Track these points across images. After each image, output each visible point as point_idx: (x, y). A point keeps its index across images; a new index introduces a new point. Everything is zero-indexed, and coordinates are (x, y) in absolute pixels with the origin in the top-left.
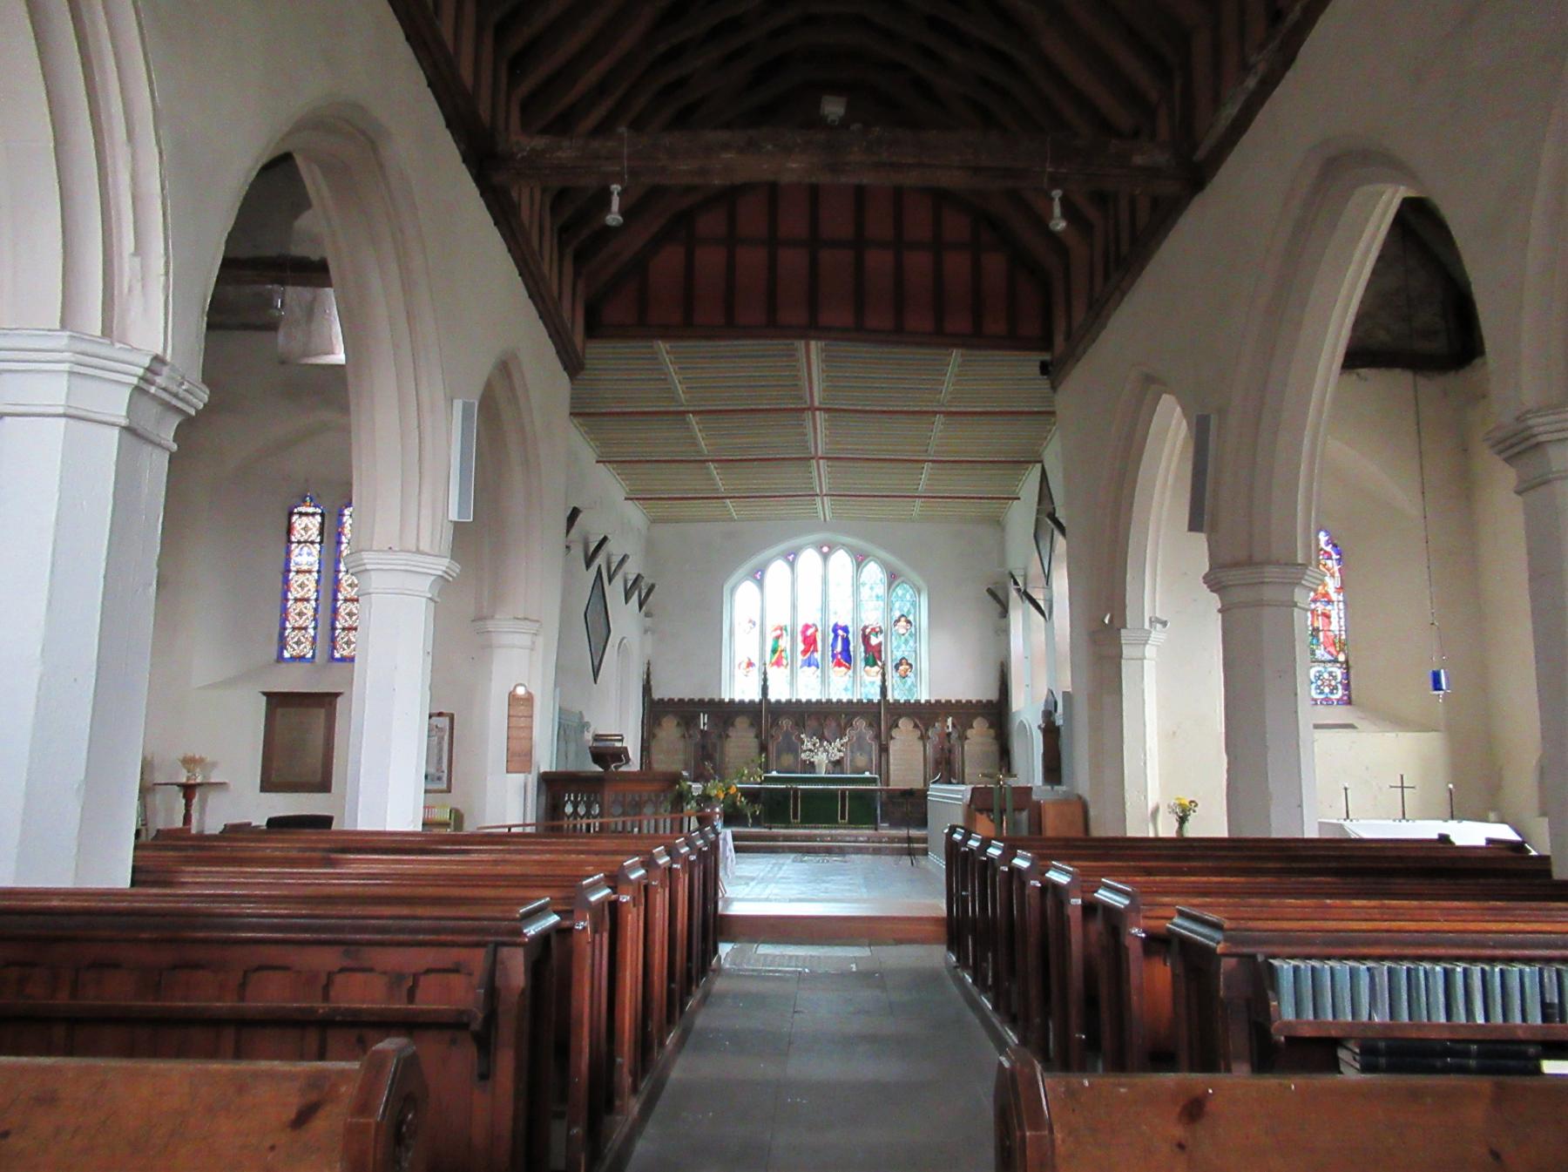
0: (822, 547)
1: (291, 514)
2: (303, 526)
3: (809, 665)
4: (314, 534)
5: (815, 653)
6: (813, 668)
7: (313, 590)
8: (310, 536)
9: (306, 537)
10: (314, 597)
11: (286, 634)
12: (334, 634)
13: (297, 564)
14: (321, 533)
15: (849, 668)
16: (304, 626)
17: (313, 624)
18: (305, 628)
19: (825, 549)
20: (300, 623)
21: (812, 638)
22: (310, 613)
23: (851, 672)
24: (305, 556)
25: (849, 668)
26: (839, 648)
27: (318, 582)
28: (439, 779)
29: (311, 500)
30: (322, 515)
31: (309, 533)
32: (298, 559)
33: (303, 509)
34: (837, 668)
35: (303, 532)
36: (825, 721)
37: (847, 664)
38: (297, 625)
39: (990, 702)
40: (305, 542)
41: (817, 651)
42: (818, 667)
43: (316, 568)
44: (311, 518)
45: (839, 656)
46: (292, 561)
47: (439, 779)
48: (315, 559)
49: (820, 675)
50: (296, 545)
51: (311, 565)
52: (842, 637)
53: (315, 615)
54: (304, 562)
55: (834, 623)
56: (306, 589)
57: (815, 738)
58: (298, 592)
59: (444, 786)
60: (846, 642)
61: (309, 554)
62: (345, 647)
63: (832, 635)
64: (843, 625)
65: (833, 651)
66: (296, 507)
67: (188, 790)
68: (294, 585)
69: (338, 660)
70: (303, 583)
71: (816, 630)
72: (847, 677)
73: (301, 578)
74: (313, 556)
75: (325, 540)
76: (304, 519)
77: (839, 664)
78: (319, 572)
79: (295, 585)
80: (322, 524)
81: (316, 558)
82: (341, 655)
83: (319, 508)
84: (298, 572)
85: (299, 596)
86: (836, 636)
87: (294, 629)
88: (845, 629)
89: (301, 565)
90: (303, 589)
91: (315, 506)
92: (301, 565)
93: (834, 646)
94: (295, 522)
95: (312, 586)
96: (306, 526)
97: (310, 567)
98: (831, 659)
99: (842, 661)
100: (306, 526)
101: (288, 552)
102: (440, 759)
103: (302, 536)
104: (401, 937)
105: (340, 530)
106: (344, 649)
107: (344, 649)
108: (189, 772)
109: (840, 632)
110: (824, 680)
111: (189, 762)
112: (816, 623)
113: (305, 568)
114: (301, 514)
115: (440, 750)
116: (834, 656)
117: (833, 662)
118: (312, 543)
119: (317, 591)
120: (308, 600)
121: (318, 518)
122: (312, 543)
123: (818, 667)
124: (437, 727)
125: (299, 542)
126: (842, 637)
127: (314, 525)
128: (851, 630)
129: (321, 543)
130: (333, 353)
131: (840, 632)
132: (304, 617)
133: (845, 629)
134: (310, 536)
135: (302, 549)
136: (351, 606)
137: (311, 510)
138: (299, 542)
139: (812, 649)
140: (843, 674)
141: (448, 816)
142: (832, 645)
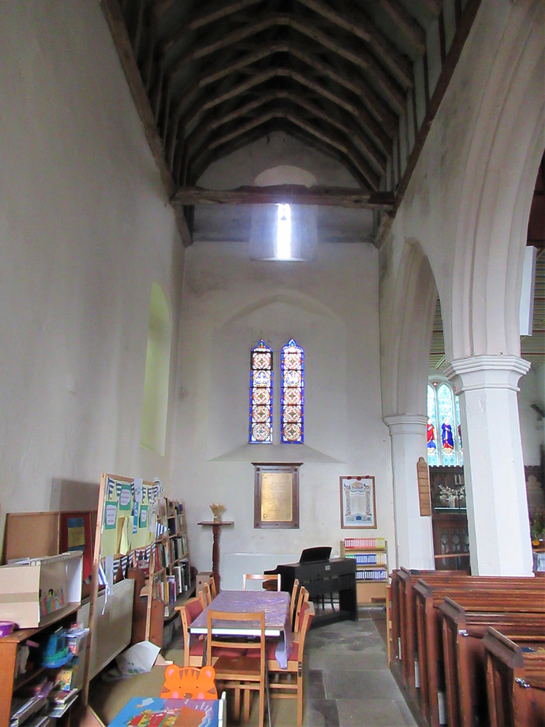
0: (434, 383)
1: (253, 352)
2: (260, 360)
3: (430, 447)
4: (267, 365)
5: (433, 441)
6: (433, 448)
7: (268, 399)
8: (264, 366)
9: (262, 367)
10: (269, 403)
11: (253, 427)
12: (283, 426)
13: (257, 383)
14: (271, 364)
15: (453, 449)
16: (263, 421)
17: (269, 420)
18: (265, 422)
19: (435, 384)
20: (261, 419)
21: (431, 432)
22: (267, 413)
23: (454, 451)
24: (262, 378)
25: (453, 449)
26: (446, 438)
27: (271, 394)
28: (369, 519)
29: (264, 345)
30: (271, 353)
31: (264, 364)
32: (258, 380)
33: (257, 350)
34: (446, 449)
35: (260, 364)
36: (445, 477)
37: (451, 446)
38: (259, 421)
39: (536, 467)
40: (262, 369)
41: (434, 439)
42: (435, 448)
43: (269, 385)
44: (264, 355)
45: (447, 442)
46: (254, 381)
47: (369, 519)
48: (268, 379)
49: (437, 452)
50: (298, 369)
51: (266, 383)
52: (448, 431)
53: (270, 414)
54: (262, 382)
55: (443, 423)
56: (264, 398)
57: (447, 487)
58: (259, 400)
59: (372, 525)
60: (450, 434)
61: (264, 377)
62: (290, 434)
63: (442, 430)
64: (448, 425)
65: (443, 439)
66: (255, 349)
67: (216, 528)
68: (256, 396)
69: (286, 442)
70: (261, 394)
71: (433, 428)
72: (452, 453)
73: (260, 391)
74: (267, 378)
75: (274, 368)
76: (261, 356)
77: (448, 447)
78: (271, 388)
79: (257, 396)
80: (272, 358)
81: (269, 379)
82: (288, 439)
83: (269, 349)
84: (258, 388)
85: (259, 403)
86: (444, 431)
87: (257, 423)
88: (449, 427)
89: (260, 383)
90: (261, 398)
91: (267, 348)
92: (260, 383)
93: (443, 436)
94: (255, 358)
95: (267, 396)
96: (262, 360)
97: (265, 385)
98: (442, 443)
99: (448, 444)
100: (262, 360)
101: (252, 376)
102: (368, 506)
103: (259, 366)
104: (420, 636)
105: (282, 362)
106: (289, 436)
107: (289, 436)
108: (215, 516)
109: (446, 429)
110: (441, 457)
111: (216, 510)
112: (451, 425)
113: (262, 385)
114: (258, 353)
115: (368, 500)
116: (444, 442)
117: (443, 445)
118: (266, 370)
119: (271, 399)
120: (265, 405)
121: (269, 355)
122: (266, 370)
123: (435, 448)
124: (365, 485)
125: (258, 370)
126: (448, 431)
127: (297, 359)
128: (452, 427)
129: (271, 370)
130: (274, 257)
131: (446, 429)
132: (263, 416)
133: (449, 427)
134: (264, 366)
135: (260, 373)
136: (293, 409)
137: (264, 350)
138: (258, 370)
139: (431, 438)
140: (449, 452)
141: (384, 545)
142: (442, 436)
